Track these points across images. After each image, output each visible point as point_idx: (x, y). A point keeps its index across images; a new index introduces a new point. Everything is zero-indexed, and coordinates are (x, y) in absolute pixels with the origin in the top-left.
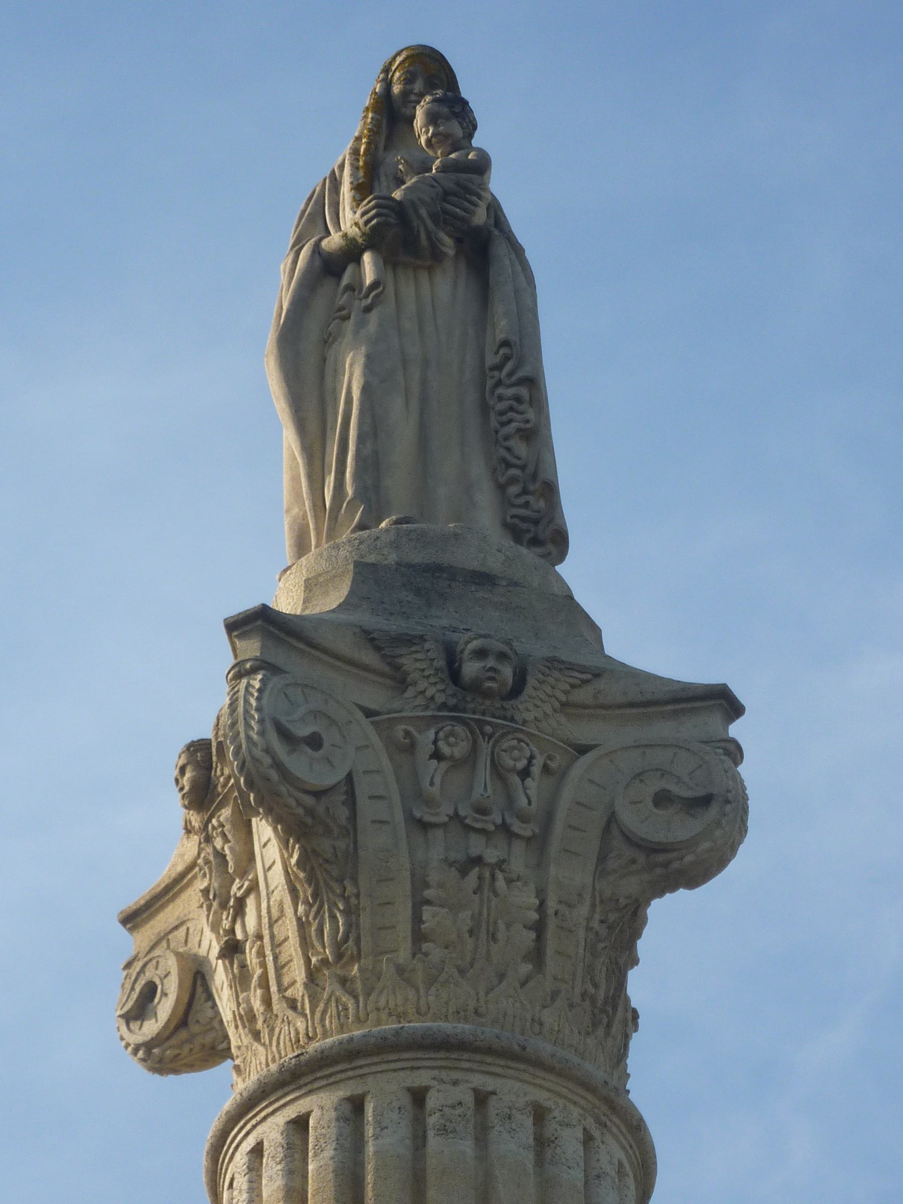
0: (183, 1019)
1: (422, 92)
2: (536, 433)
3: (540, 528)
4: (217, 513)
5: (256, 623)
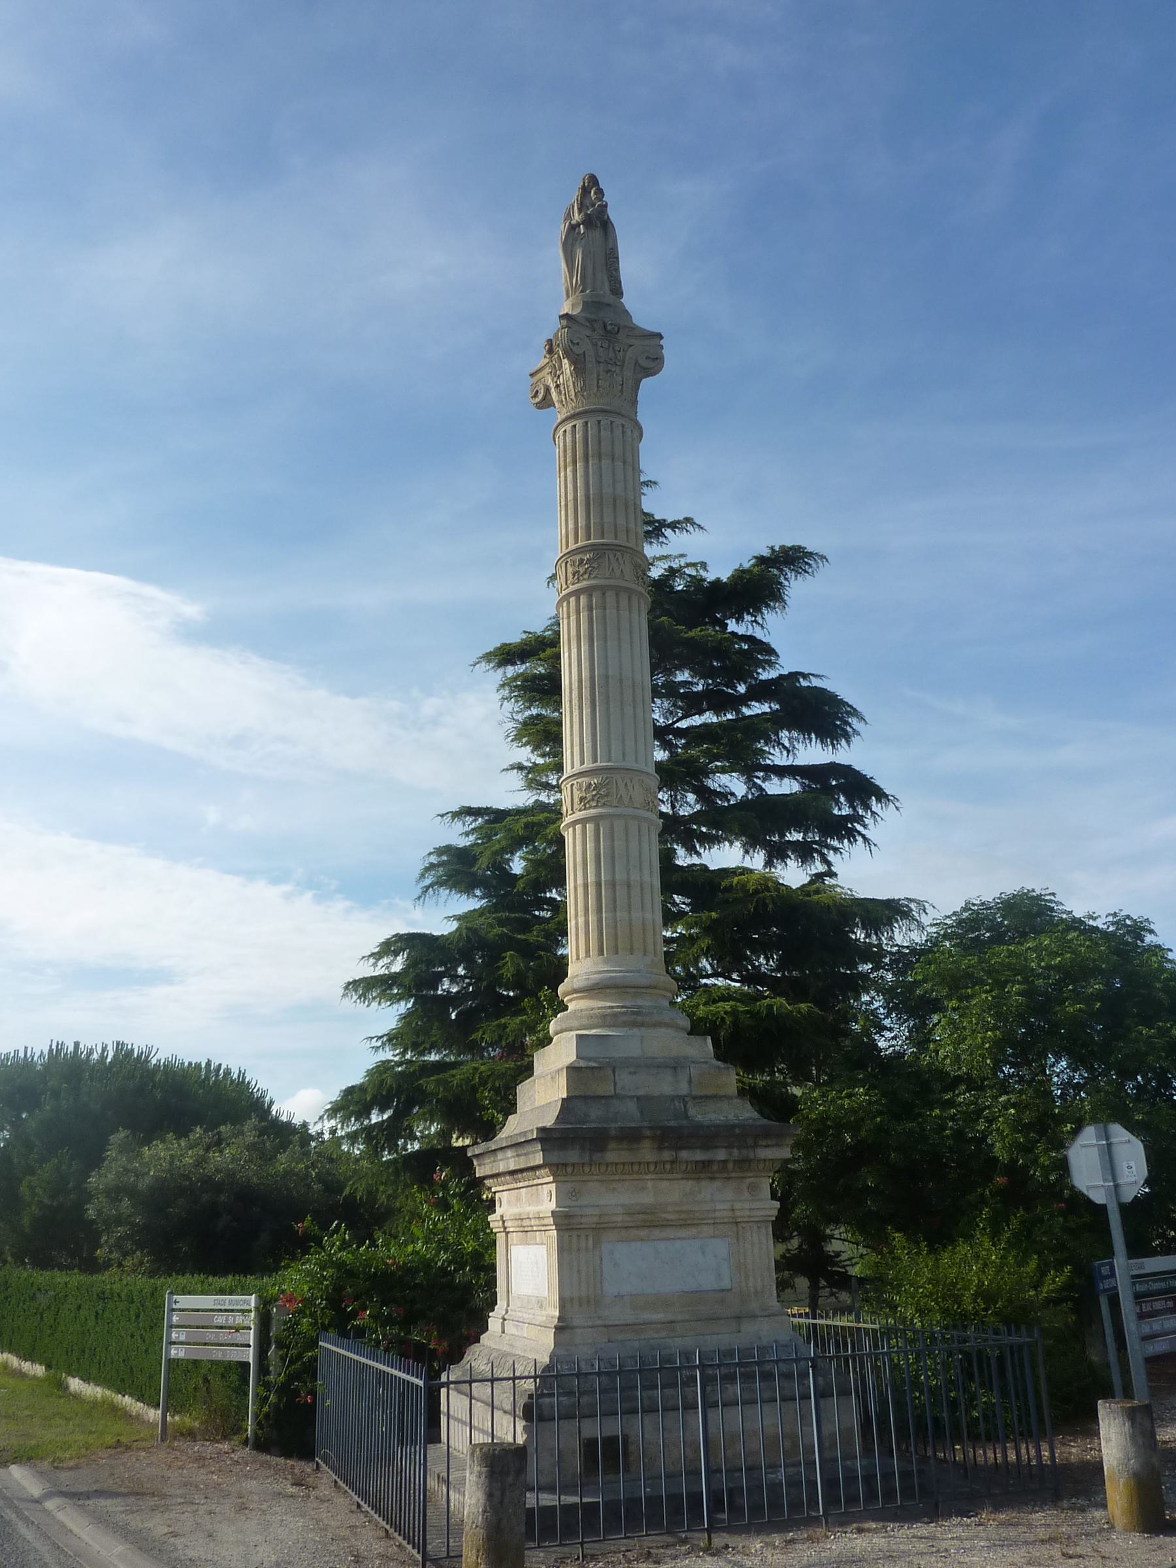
0: (544, 399)
1: (592, 184)
2: (617, 270)
3: (617, 291)
4: (555, 294)
5: (566, 316)
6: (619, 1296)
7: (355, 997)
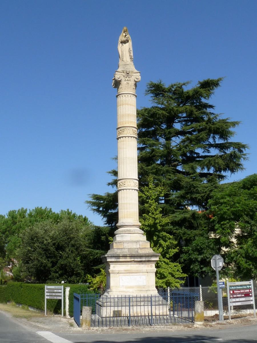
6: (123, 286)
7: (93, 224)
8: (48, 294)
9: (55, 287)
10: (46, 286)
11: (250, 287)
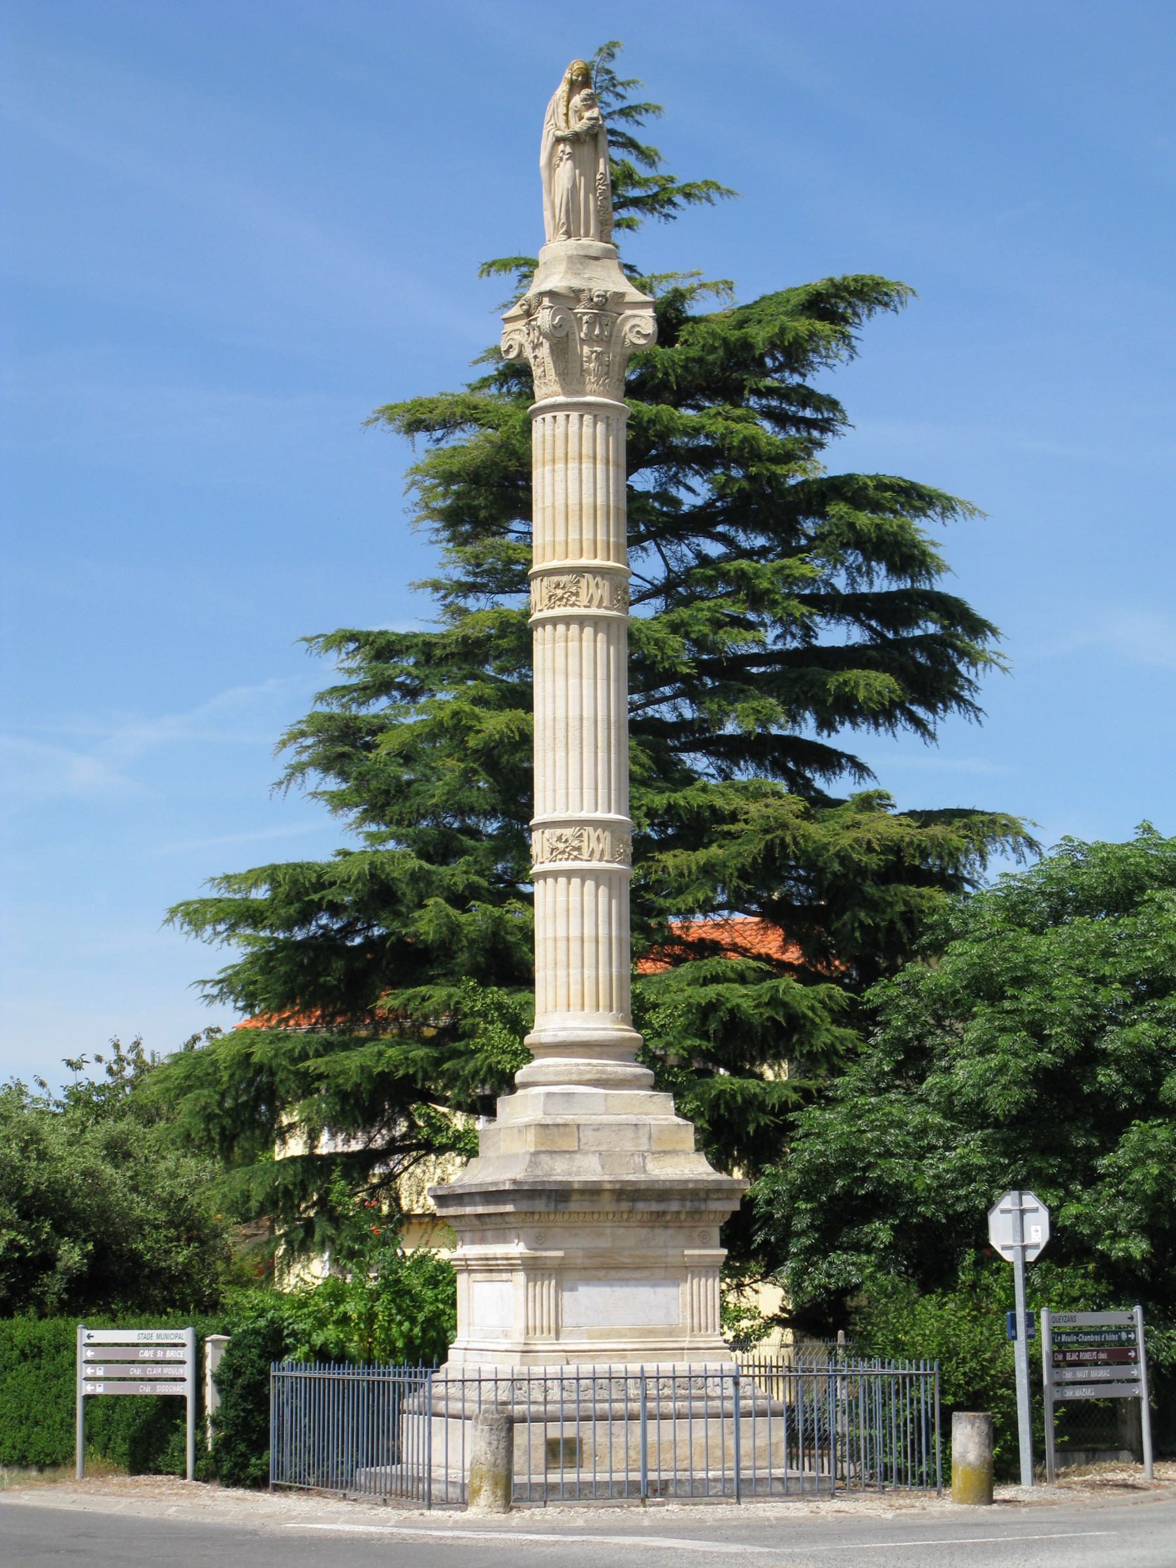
8: (100, 1371)
9: (158, 1336)
10: (83, 1335)
11: (1132, 1336)
